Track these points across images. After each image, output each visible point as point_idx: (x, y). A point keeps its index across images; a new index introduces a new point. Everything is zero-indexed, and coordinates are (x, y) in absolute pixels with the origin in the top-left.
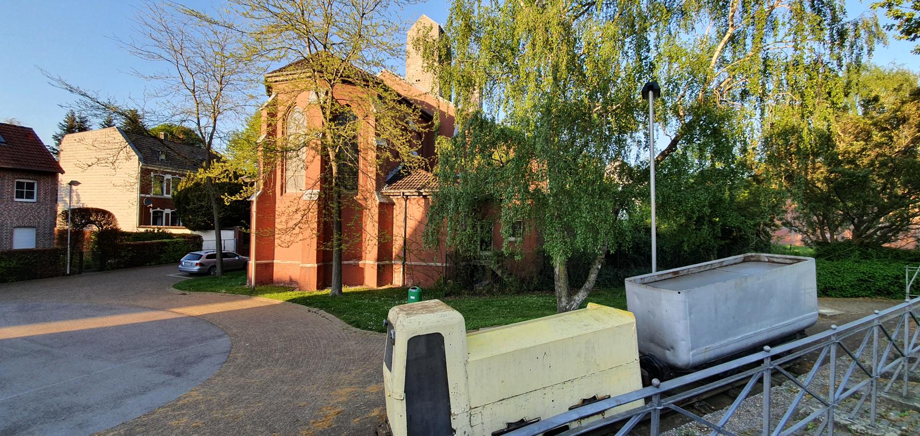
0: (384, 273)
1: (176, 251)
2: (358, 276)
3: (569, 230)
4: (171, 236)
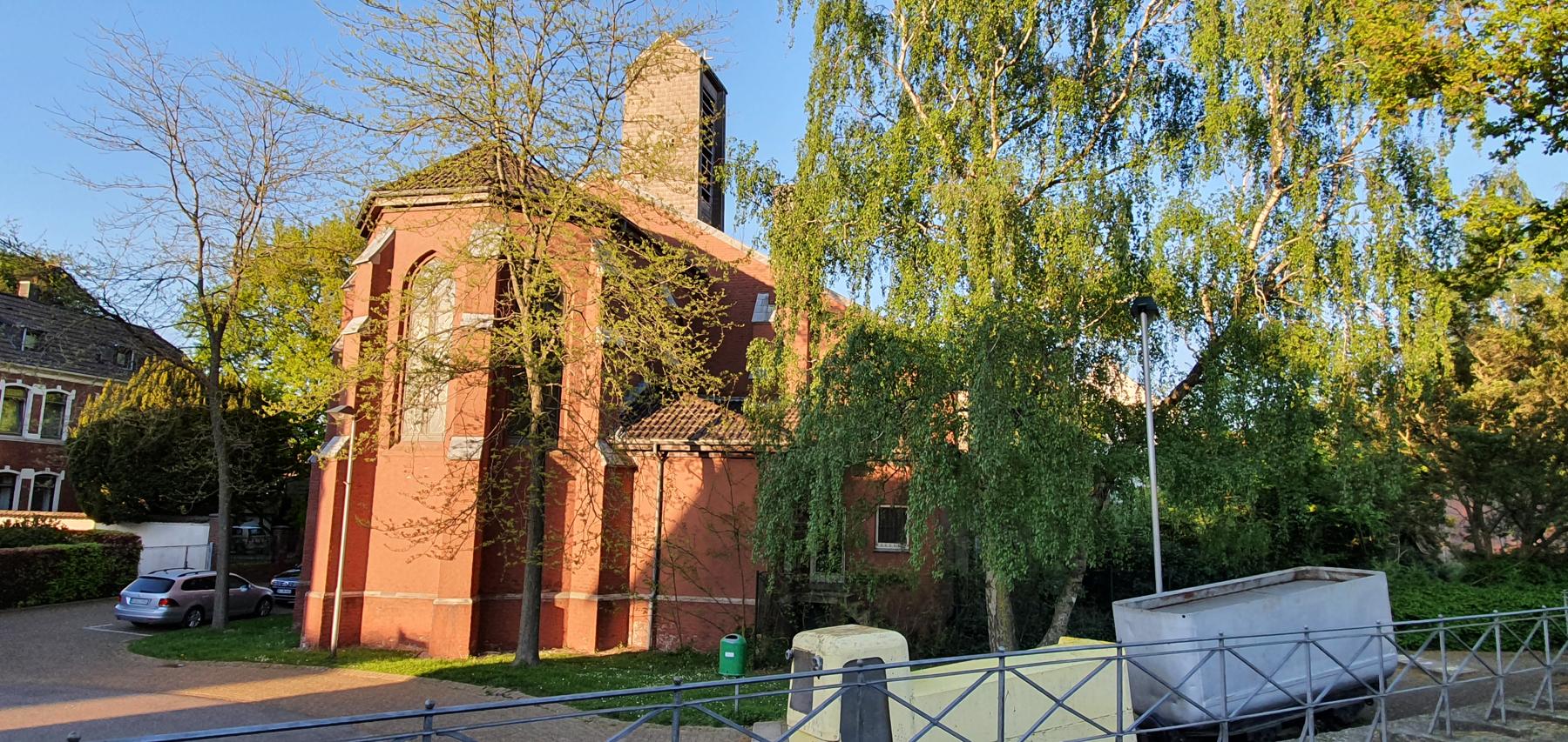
0: (610, 622)
1: (83, 574)
2: (549, 624)
3: (1021, 527)
4: (65, 535)
